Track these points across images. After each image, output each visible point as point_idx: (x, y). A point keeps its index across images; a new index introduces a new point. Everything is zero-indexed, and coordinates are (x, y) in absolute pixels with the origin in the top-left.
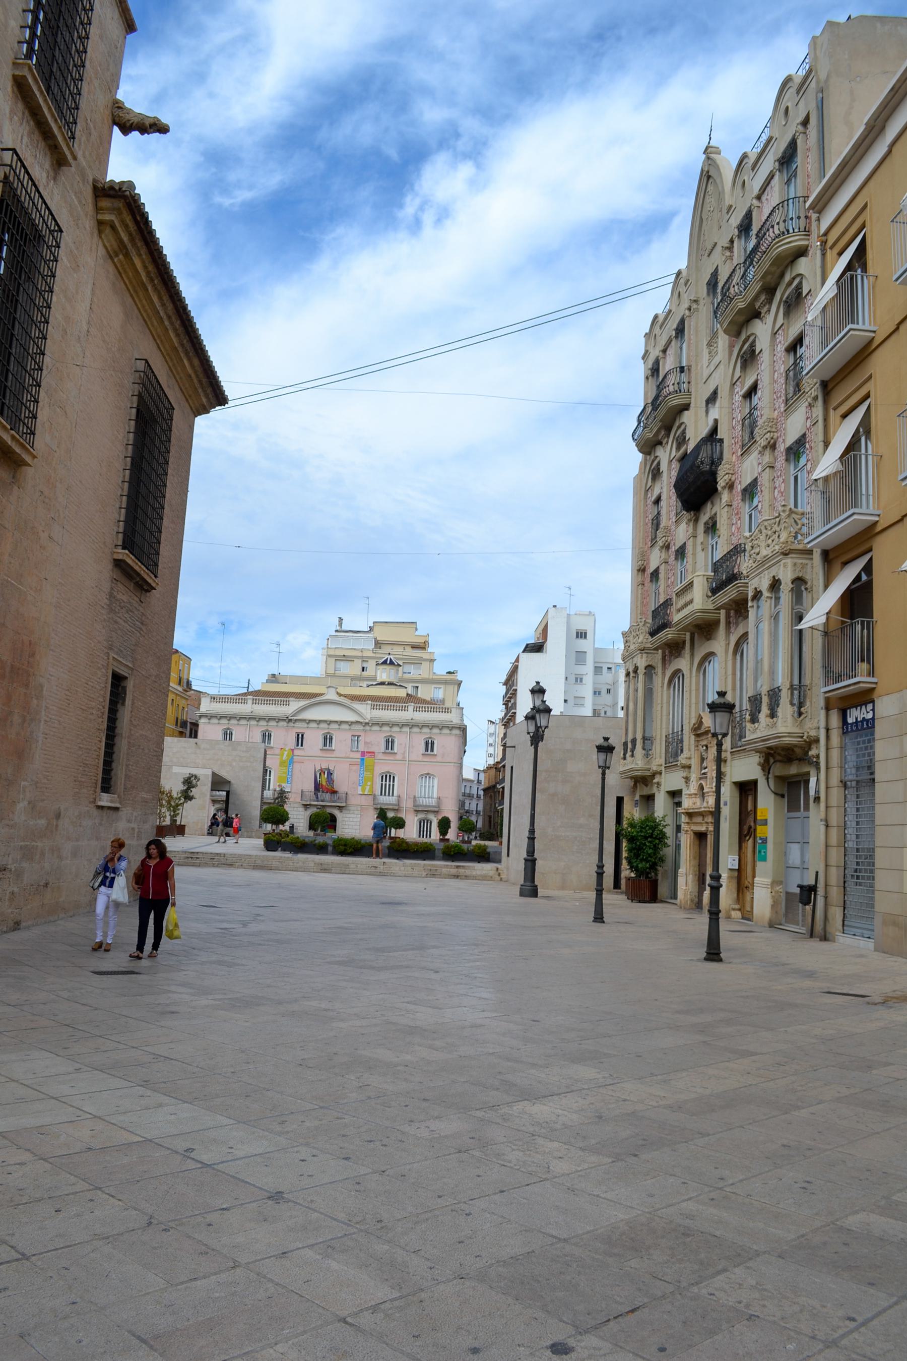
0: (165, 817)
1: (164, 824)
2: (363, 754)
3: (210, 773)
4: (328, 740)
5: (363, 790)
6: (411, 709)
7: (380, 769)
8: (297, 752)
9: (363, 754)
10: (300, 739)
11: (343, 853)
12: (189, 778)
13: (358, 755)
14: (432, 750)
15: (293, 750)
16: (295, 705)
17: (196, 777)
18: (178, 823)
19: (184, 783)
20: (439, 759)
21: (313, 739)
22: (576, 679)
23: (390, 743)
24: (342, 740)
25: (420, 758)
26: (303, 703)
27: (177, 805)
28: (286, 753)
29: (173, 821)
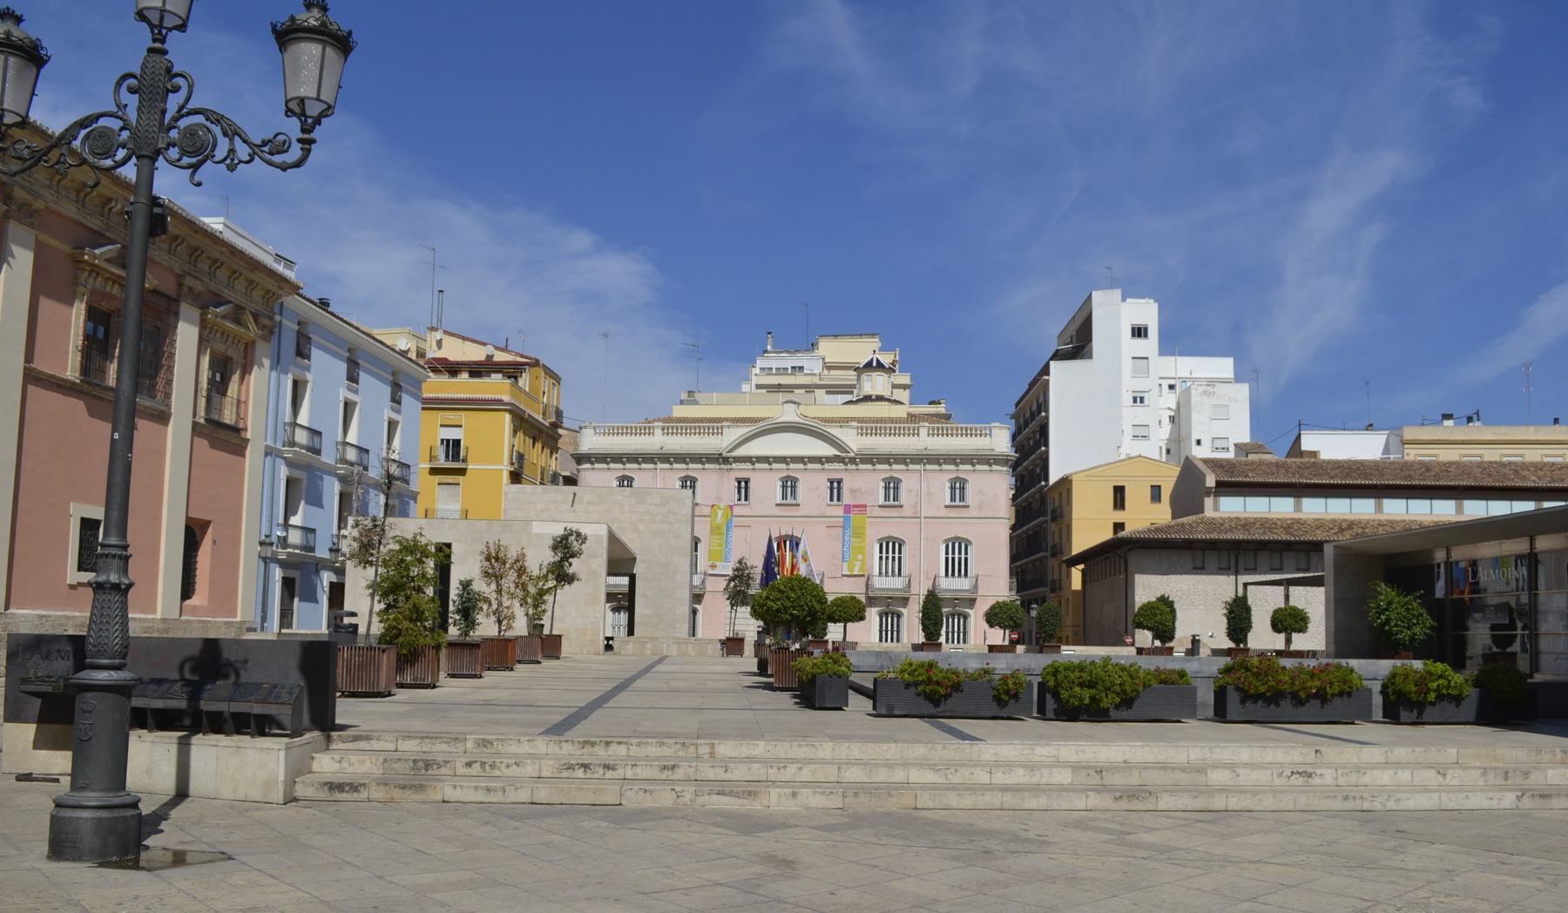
0: (512, 617)
1: (510, 634)
2: (848, 509)
3: (605, 533)
4: (789, 485)
5: (851, 568)
6: (923, 432)
7: (876, 530)
8: (737, 511)
9: (848, 509)
10: (743, 486)
11: (1069, 713)
12: (565, 538)
13: (840, 511)
14: (962, 498)
15: (731, 507)
16: (732, 435)
17: (579, 535)
18: (546, 631)
19: (554, 548)
20: (973, 512)
21: (766, 485)
22: (1135, 400)
23: (892, 486)
24: (813, 485)
26: (741, 431)
27: (542, 593)
28: (720, 513)
29: (536, 627)
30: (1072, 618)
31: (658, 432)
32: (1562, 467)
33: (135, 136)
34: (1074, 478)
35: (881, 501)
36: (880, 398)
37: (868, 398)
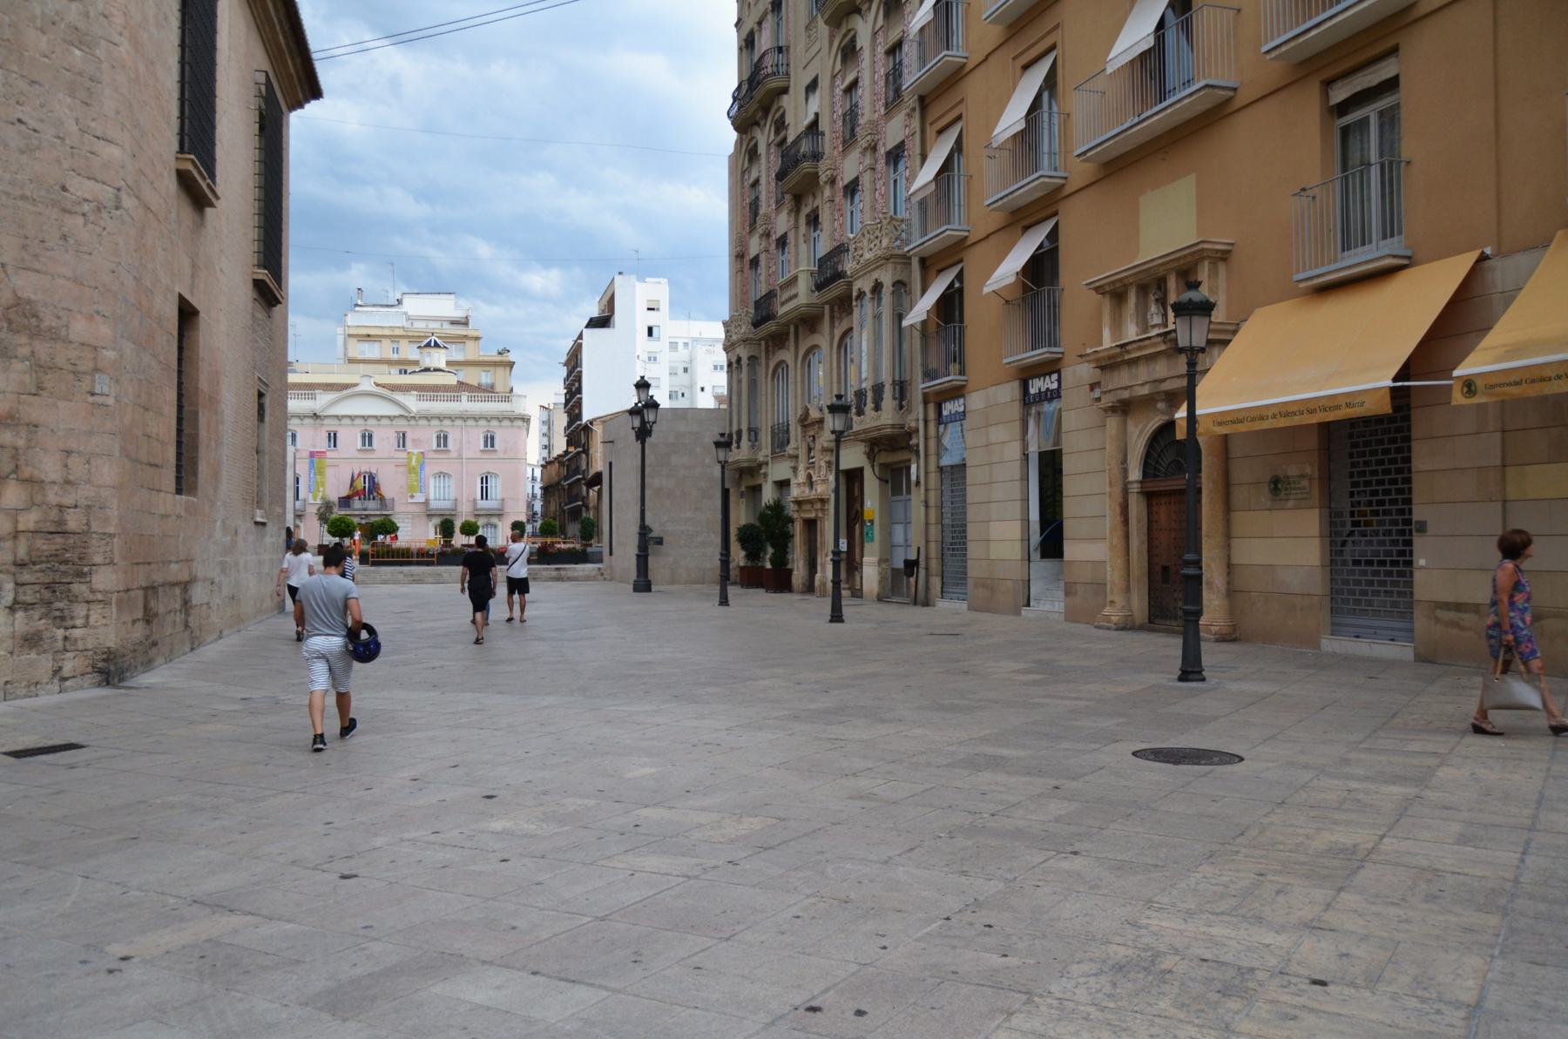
4: (368, 438)
6: (464, 398)
21: (350, 438)
23: (443, 440)
24: (384, 439)
25: (479, 455)
30: (1147, 968)
31: (464, 398)
32: (1567, 371)
33: (778, 507)
34: (1535, 539)
35: (434, 447)
36: (436, 370)
37: (427, 370)
